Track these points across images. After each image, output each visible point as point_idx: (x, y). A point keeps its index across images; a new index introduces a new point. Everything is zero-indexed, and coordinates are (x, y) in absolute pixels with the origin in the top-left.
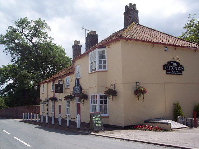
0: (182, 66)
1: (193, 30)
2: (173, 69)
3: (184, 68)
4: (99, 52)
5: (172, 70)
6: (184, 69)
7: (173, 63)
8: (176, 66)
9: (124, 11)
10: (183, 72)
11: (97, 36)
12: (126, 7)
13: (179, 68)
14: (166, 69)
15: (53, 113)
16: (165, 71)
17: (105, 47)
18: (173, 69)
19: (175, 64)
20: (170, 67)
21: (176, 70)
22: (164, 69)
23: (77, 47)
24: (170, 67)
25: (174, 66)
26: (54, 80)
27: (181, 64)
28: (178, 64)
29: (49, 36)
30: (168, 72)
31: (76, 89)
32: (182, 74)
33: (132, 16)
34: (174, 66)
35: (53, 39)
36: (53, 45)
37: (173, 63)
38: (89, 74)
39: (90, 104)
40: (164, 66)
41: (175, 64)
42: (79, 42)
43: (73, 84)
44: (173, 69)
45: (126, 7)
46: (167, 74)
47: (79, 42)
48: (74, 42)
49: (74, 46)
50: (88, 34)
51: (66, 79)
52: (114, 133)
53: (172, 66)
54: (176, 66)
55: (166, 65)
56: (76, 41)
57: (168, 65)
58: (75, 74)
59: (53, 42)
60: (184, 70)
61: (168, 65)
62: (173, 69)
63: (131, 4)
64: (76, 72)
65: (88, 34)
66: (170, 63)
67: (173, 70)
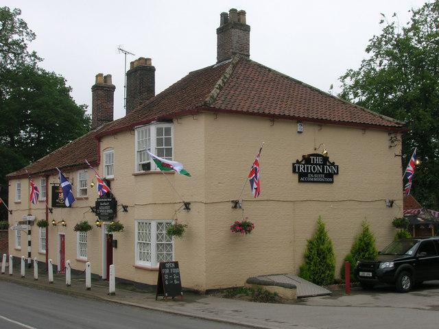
0: (333, 164)
1: (388, 53)
2: (314, 170)
3: (337, 168)
4: (159, 132)
5: (311, 173)
6: (337, 171)
7: (314, 159)
8: (319, 165)
9: (218, 26)
10: (335, 177)
11: (152, 70)
12: (224, 16)
13: (328, 169)
14: (299, 173)
15: (45, 252)
16: (296, 176)
17: (170, 121)
18: (314, 170)
19: (319, 160)
20: (308, 168)
21: (320, 173)
22: (294, 171)
23: (103, 89)
24: (308, 168)
25: (316, 164)
26: (49, 173)
27: (331, 160)
28: (325, 159)
29: (30, 50)
30: (303, 177)
31: (103, 202)
32: (332, 182)
33: (235, 39)
34: (316, 164)
35: (39, 59)
36: (40, 72)
37: (314, 159)
38: (136, 175)
39: (137, 241)
40: (294, 164)
41: (319, 160)
42: (108, 77)
43: (94, 195)
44: (314, 170)
45: (224, 16)
46: (300, 181)
47: (108, 77)
48: (97, 76)
49: (95, 89)
50: (132, 63)
51: (78, 179)
52: (430, 296)
53: (312, 164)
54: (319, 165)
55: (298, 162)
56: (100, 75)
57: (303, 163)
58: (103, 172)
59: (40, 65)
60: (337, 173)
61: (303, 163)
62: (314, 170)
63: (233, 11)
64: (105, 164)
65: (132, 63)
66: (307, 160)
67: (314, 174)
